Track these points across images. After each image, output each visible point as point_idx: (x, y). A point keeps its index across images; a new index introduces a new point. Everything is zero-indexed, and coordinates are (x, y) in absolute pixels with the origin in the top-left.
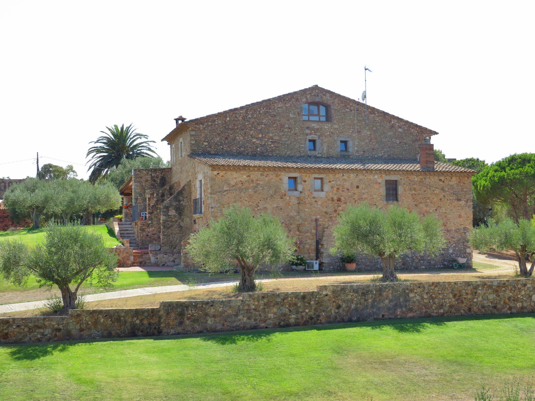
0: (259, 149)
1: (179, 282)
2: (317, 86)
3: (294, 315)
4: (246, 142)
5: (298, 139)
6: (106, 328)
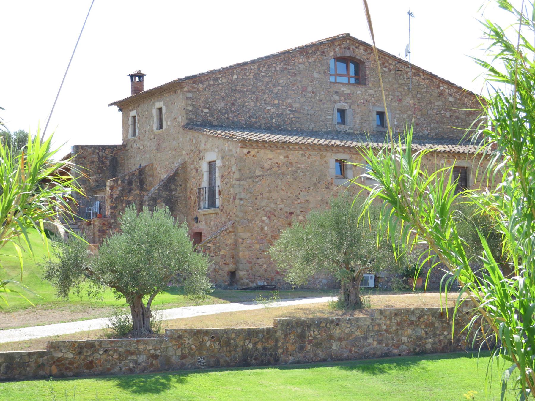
0: (274, 121)
1: (227, 302)
2: (348, 35)
3: (431, 338)
4: (257, 110)
5: (324, 108)
6: (213, 354)
